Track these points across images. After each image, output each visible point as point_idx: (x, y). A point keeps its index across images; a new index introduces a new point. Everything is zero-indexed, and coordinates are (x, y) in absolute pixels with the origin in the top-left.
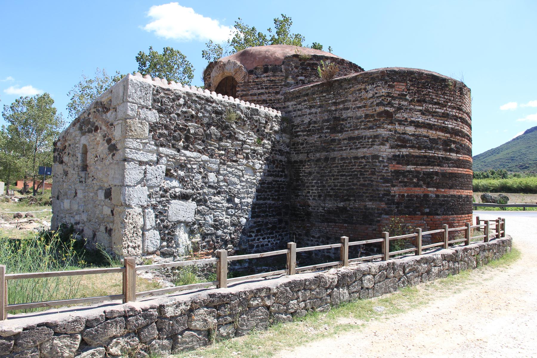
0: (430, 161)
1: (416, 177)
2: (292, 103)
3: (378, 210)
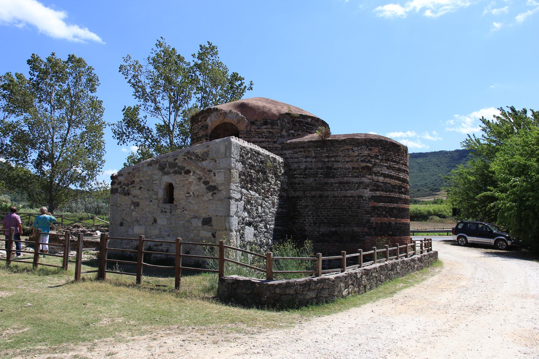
0: (392, 200)
1: (385, 210)
2: (289, 152)
3: (362, 232)
